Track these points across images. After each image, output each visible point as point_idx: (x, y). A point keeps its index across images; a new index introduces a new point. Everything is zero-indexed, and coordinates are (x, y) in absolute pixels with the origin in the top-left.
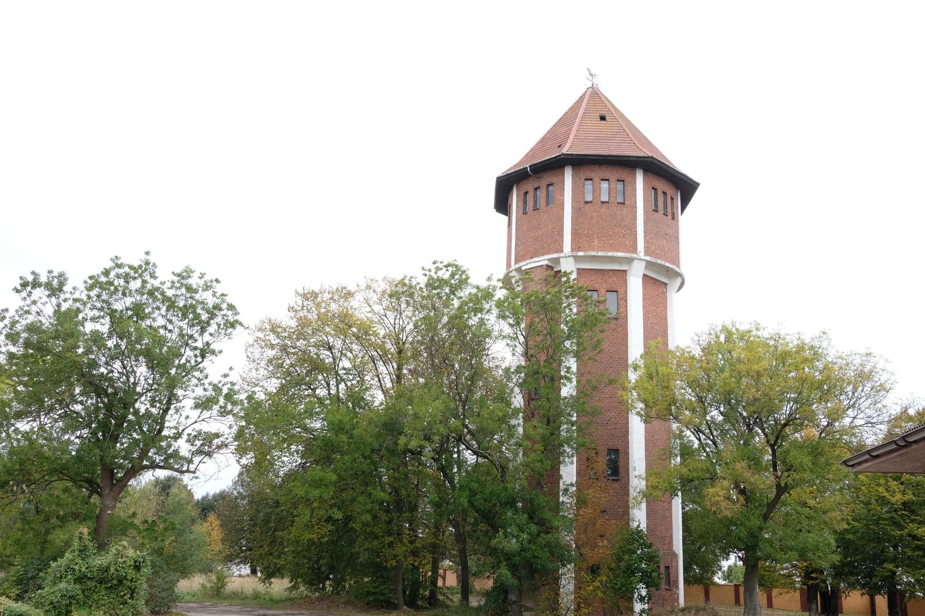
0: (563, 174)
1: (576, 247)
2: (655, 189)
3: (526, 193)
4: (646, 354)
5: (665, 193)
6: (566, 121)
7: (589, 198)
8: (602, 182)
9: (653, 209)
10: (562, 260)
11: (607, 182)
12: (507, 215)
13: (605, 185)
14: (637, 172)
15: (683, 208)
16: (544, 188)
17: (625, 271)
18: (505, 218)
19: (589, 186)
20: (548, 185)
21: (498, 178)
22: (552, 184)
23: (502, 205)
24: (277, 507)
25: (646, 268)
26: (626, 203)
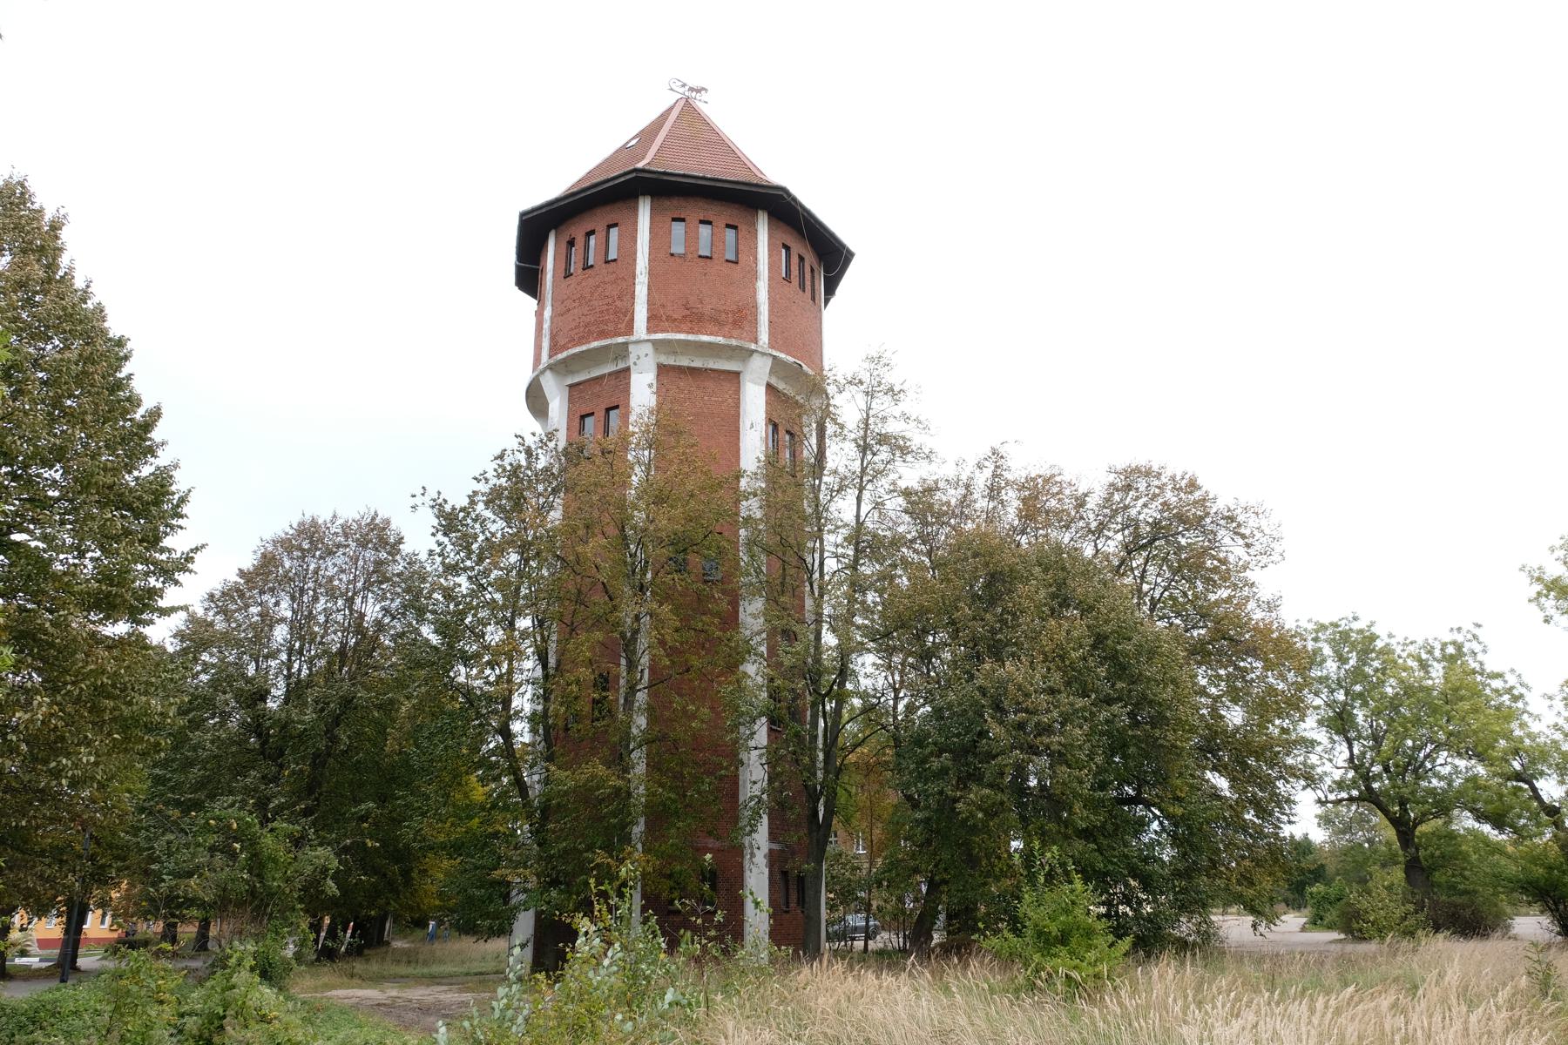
0: (637, 215)
1: (654, 322)
2: (787, 248)
3: (571, 243)
4: (772, 460)
5: (801, 259)
6: (648, 135)
7: (678, 249)
8: (701, 225)
9: (781, 280)
10: (631, 348)
11: (710, 227)
12: (535, 297)
13: (705, 231)
14: (760, 212)
15: (827, 301)
16: (601, 234)
17: (737, 374)
18: (532, 303)
19: (678, 229)
20: (608, 410)
21: (522, 215)
22: (617, 407)
23: (528, 279)
24: (53, 1015)
25: (772, 372)
26: (740, 261)
